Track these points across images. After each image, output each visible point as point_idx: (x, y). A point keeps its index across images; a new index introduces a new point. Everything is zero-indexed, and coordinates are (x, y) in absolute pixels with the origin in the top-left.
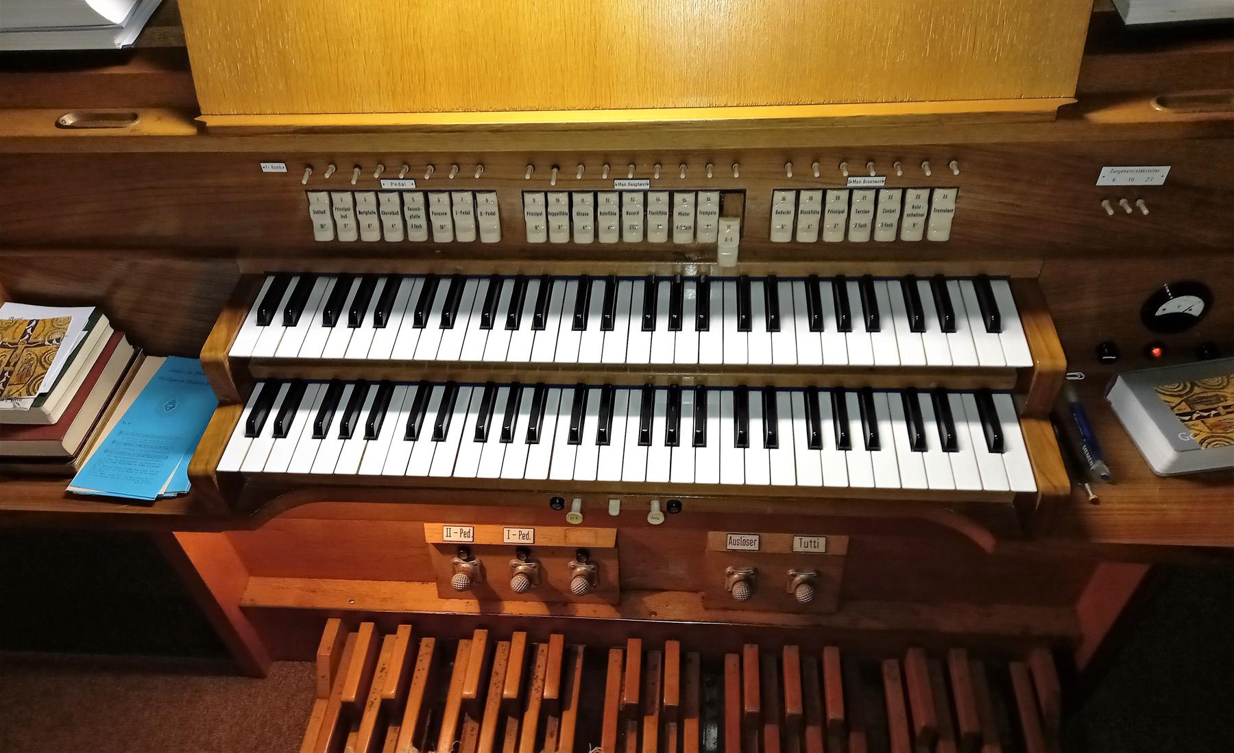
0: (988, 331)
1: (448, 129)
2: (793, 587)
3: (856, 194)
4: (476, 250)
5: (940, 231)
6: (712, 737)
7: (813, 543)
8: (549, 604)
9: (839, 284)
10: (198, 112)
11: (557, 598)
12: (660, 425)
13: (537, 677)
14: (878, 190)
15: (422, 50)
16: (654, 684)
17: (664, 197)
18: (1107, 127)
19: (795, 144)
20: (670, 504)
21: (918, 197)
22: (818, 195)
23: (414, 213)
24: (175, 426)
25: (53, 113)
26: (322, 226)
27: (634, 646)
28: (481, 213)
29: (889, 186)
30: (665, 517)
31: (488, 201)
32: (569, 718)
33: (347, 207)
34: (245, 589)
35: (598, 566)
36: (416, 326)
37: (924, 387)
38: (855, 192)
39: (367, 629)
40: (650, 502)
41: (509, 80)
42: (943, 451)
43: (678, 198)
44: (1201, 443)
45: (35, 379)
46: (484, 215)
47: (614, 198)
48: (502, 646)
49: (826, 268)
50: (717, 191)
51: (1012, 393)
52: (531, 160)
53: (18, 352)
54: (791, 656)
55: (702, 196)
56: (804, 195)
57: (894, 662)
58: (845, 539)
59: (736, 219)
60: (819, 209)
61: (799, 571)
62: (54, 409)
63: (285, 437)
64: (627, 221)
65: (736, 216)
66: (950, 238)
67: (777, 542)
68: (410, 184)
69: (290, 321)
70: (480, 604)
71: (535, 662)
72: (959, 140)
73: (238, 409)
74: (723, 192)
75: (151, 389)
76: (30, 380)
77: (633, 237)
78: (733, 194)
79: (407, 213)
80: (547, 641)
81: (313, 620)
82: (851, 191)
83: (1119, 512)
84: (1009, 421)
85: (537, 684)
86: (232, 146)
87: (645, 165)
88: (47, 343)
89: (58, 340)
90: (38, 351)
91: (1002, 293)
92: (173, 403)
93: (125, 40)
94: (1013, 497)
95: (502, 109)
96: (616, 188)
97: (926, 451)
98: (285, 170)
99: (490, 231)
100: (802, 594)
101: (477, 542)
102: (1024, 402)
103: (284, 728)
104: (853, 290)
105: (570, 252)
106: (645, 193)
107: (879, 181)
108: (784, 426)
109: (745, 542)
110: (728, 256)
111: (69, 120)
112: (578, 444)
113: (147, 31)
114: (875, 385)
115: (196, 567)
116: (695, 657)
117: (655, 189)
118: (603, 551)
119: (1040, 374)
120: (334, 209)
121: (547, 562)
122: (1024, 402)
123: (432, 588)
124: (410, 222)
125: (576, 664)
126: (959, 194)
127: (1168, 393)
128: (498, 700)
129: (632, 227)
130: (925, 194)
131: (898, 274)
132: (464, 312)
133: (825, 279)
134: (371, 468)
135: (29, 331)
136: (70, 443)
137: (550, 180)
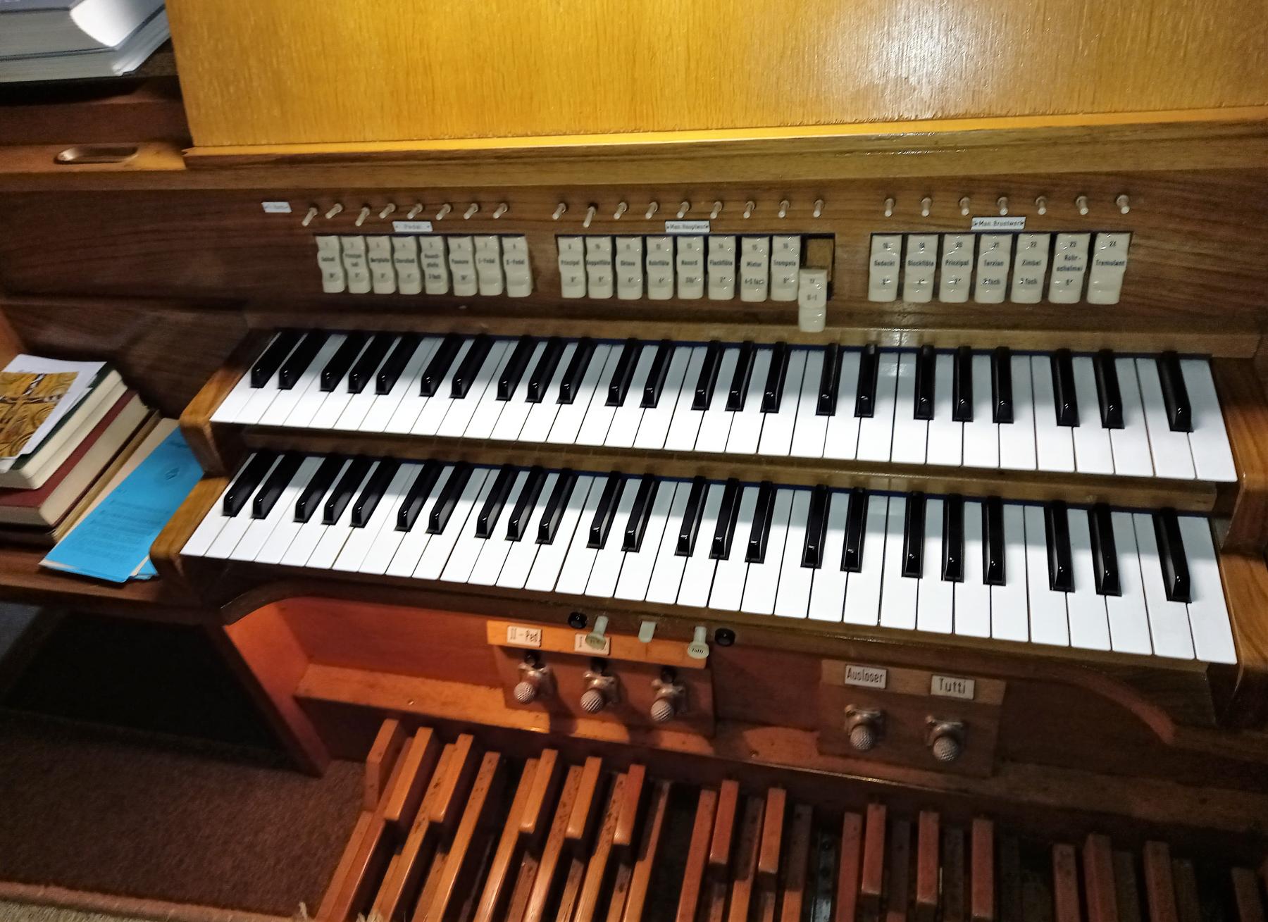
0: (1173, 428)
1: (446, 156)
2: (932, 738)
3: (986, 241)
4: (502, 306)
5: (1106, 290)
6: (824, 916)
7: (957, 686)
8: (631, 728)
9: (963, 360)
10: (189, 144)
11: (638, 722)
12: (707, 530)
13: (610, 815)
14: (1015, 235)
15: (430, 65)
16: (751, 841)
17: (730, 243)
19: (894, 173)
20: (719, 634)
21: (1073, 244)
22: (932, 241)
23: (432, 261)
24: (156, 499)
25: (52, 149)
26: (332, 275)
27: (730, 789)
28: (508, 261)
29: (1031, 229)
30: (711, 650)
31: (518, 247)
32: (643, 870)
33: (357, 253)
34: (302, 677)
35: (688, 689)
36: (423, 394)
37: (1079, 500)
38: (984, 238)
39: (423, 736)
40: (694, 628)
41: (531, 98)
42: (1098, 593)
43: (747, 244)
45: (22, 438)
46: (511, 264)
47: (667, 243)
48: (573, 771)
49: (984, 338)
50: (797, 235)
51: (1211, 517)
52: (563, 195)
53: (15, 408)
54: (928, 825)
55: (778, 242)
56: (913, 241)
57: (1069, 849)
58: (1001, 685)
59: (822, 270)
60: (933, 259)
61: (941, 719)
62: (38, 472)
63: (264, 518)
64: (683, 272)
65: (822, 268)
66: (1120, 301)
67: (909, 681)
68: (426, 227)
69: (458, 392)
71: (611, 797)
72: (1127, 165)
73: (222, 482)
74: (805, 239)
75: (157, 454)
76: (16, 437)
77: (690, 292)
78: (819, 240)
79: (425, 261)
80: (626, 771)
81: (369, 718)
82: (978, 235)
84: (1202, 556)
85: (608, 824)
86: (225, 182)
87: (703, 203)
88: (46, 399)
89: (59, 397)
90: (35, 407)
91: (1198, 378)
92: (176, 470)
93: (125, 67)
94: (1206, 667)
95: (524, 133)
96: (668, 231)
97: (1072, 590)
98: (288, 210)
99: (520, 283)
100: (942, 750)
101: (545, 647)
102: (1224, 528)
103: (333, 838)
104: (982, 370)
105: (613, 310)
106: (706, 238)
107: (1017, 223)
108: (872, 543)
109: (867, 678)
110: (812, 319)
111: (68, 155)
112: (599, 548)
113: (158, 57)
114: (1007, 495)
116: (805, 812)
117: (718, 233)
118: (692, 672)
119: (1247, 493)
120: (344, 255)
121: (626, 678)
122: (1224, 528)
123: (499, 694)
124: (428, 271)
126: (1133, 241)
128: (561, 839)
129: (690, 281)
130: (1084, 240)
131: (1047, 347)
132: (672, 387)
133: (982, 352)
134: (348, 564)
135: (33, 385)
136: (50, 511)
137: (583, 221)
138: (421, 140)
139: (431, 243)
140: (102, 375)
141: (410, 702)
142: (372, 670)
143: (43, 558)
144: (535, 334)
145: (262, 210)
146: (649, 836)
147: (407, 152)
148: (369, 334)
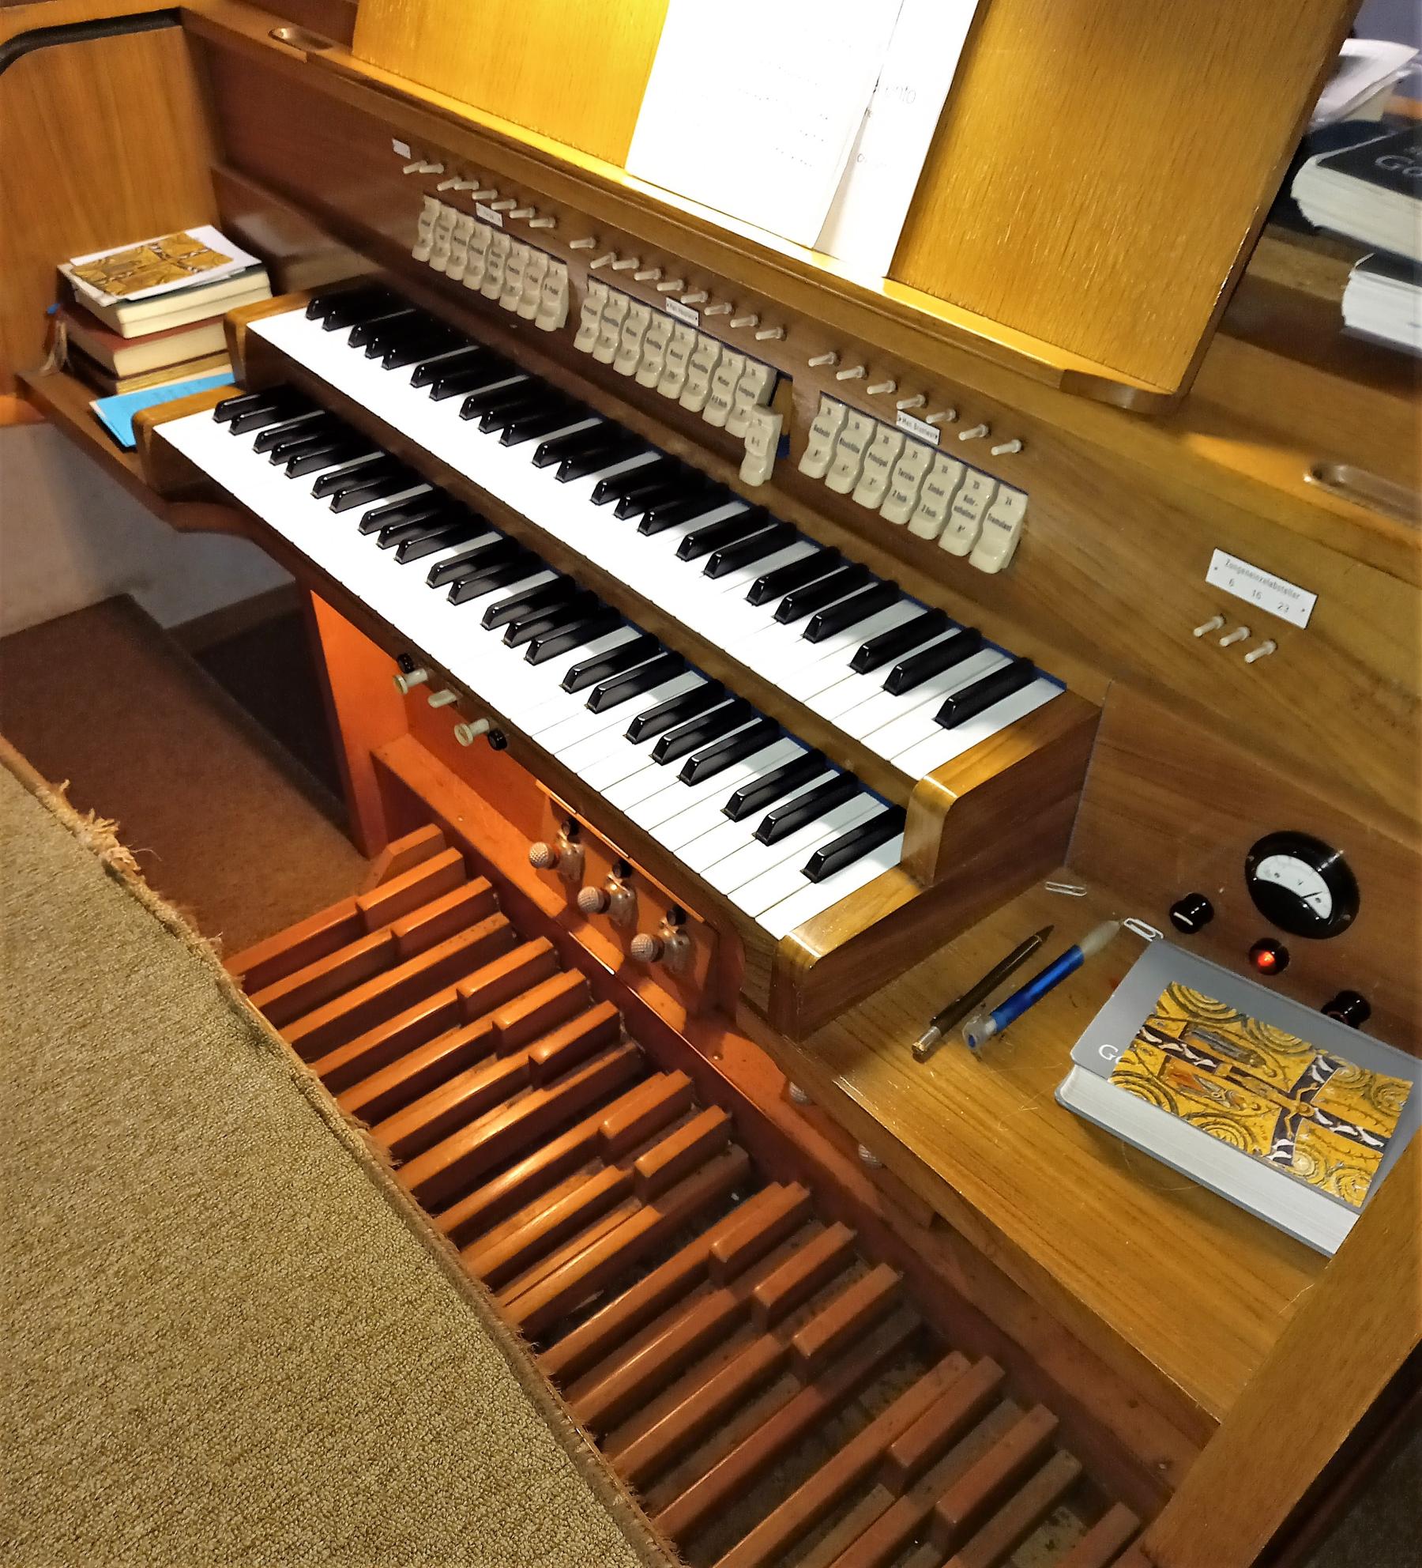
18: (1205, 465)
44: (1117, 1074)
70: (564, 910)
79: (959, 501)
83: (931, 1089)
111: (285, 33)
115: (330, 667)
125: (607, 1055)
127: (1181, 999)
138: (445, 94)
139: (916, 453)
140: (250, 270)
141: (461, 817)
142: (454, 771)
143: (94, 399)
144: (522, 363)
145: (391, 146)
146: (573, 1075)
147: (526, 146)
148: (953, 624)
